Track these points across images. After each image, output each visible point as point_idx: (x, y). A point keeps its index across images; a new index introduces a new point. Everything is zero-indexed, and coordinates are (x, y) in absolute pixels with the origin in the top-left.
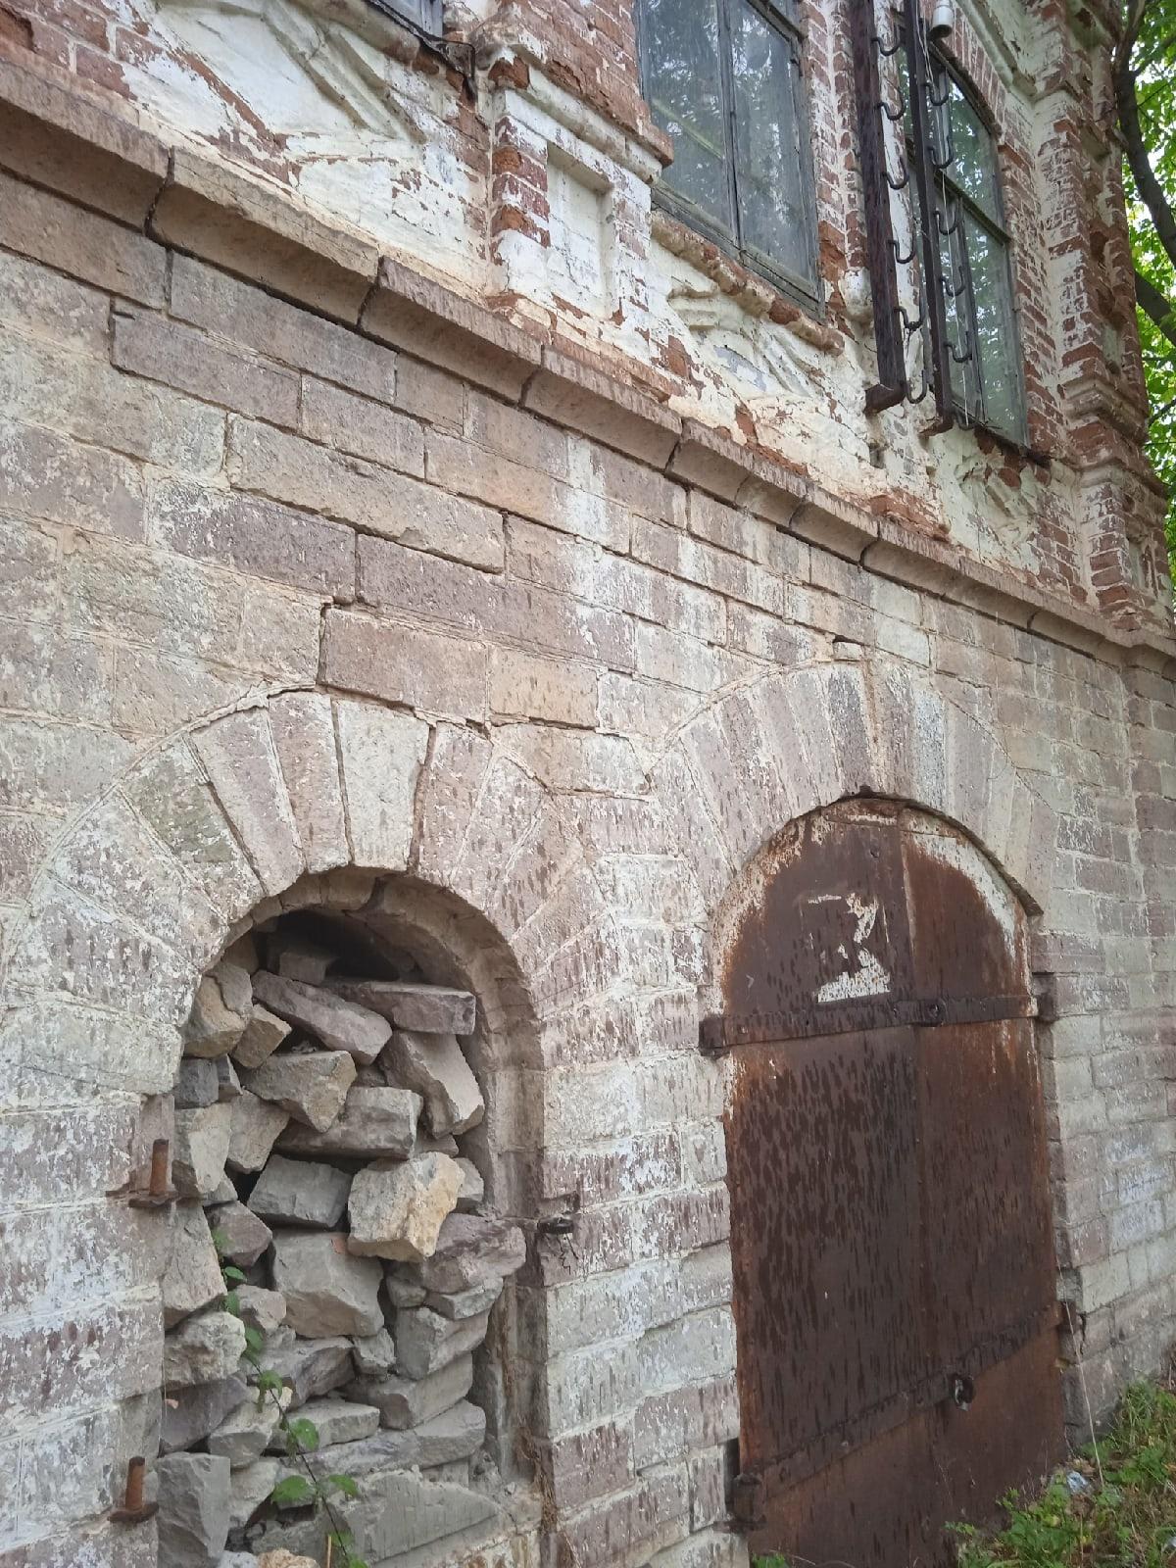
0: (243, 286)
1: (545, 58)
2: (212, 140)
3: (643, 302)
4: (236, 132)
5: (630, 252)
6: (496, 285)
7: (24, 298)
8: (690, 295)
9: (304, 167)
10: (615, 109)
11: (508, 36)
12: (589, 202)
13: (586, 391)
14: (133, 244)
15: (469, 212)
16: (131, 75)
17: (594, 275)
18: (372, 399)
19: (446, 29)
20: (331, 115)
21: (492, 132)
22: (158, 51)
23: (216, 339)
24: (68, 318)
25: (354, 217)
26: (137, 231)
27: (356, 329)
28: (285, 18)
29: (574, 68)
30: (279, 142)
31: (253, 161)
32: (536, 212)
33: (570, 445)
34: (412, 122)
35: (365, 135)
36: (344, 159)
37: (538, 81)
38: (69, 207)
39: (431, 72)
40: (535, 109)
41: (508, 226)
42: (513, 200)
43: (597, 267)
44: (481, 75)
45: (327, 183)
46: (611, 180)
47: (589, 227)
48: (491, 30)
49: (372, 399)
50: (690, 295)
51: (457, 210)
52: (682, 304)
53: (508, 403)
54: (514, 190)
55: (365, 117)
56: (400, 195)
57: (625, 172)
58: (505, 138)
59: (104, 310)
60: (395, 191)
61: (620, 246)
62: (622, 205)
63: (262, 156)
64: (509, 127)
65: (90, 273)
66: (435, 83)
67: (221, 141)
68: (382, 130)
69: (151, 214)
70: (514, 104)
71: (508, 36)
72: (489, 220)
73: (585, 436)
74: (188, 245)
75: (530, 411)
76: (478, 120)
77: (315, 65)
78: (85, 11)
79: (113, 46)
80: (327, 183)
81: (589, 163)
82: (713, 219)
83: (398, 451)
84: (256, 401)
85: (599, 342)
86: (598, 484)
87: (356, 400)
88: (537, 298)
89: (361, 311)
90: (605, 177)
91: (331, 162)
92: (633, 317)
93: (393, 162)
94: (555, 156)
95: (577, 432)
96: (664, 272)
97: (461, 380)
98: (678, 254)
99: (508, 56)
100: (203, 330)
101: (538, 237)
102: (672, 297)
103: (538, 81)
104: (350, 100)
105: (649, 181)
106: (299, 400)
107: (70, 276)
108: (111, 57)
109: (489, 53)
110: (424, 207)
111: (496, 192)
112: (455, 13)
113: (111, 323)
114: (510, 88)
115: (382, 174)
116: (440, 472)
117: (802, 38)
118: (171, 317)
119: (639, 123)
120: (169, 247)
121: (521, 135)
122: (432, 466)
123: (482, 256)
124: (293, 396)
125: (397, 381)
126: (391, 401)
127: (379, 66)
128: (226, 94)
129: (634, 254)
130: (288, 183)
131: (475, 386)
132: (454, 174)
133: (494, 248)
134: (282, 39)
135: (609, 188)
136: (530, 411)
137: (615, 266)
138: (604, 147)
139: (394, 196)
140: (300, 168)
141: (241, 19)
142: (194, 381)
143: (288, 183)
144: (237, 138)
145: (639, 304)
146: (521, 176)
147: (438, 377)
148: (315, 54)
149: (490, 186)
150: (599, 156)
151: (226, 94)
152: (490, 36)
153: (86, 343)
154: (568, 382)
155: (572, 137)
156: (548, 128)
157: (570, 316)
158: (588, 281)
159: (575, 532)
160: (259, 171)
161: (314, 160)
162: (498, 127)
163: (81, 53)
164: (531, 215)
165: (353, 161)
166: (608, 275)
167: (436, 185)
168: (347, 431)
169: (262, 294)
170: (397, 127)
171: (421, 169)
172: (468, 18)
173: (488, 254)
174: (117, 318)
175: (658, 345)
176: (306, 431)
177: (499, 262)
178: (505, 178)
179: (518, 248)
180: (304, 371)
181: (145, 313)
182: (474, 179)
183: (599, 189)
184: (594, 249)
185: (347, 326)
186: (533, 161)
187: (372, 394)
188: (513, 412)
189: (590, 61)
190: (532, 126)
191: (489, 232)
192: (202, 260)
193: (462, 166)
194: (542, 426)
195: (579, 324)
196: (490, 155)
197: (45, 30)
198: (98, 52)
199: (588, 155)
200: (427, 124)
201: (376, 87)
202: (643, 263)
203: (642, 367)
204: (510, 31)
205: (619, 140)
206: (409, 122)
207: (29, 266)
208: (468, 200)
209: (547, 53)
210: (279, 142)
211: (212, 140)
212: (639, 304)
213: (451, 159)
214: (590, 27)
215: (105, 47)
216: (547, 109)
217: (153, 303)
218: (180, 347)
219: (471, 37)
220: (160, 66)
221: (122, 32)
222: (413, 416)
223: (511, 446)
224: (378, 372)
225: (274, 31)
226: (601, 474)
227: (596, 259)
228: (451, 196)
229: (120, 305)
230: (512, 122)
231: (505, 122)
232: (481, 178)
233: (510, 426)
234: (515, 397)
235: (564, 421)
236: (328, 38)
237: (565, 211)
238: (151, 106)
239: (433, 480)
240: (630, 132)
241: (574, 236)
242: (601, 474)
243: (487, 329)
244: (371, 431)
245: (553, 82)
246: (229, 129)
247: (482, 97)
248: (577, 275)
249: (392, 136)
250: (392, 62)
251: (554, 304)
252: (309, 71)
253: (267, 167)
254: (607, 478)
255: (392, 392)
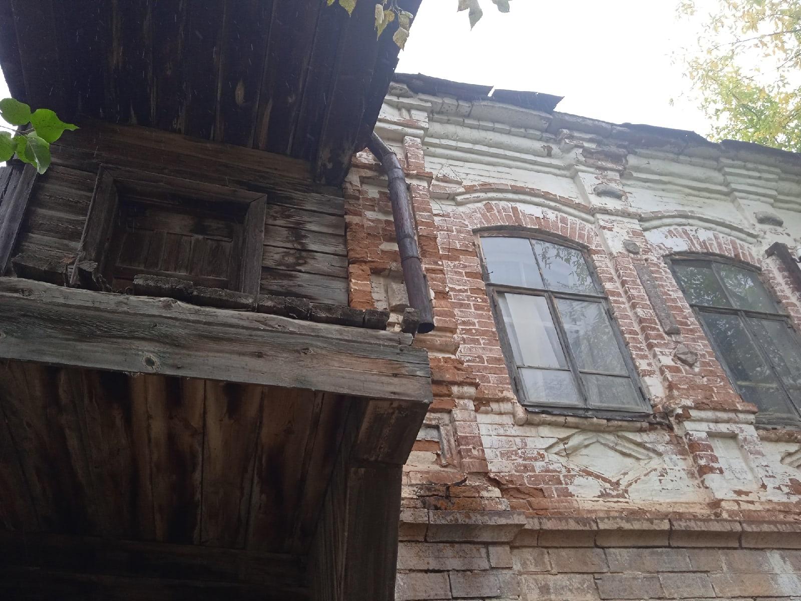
0: (628, 550)
1: (693, 404)
2: (599, 497)
3: (771, 474)
4: (605, 490)
5: (757, 456)
6: (709, 498)
7: (571, 588)
8: (790, 455)
9: (629, 489)
10: (726, 406)
11: (676, 404)
12: (731, 443)
13: (765, 532)
14: (593, 553)
15: (688, 473)
16: (571, 488)
17: (746, 472)
18: (684, 572)
19: (653, 406)
20: (629, 461)
21: (684, 438)
22: (575, 475)
23: (627, 574)
24: (584, 588)
25: (650, 498)
26: (592, 547)
27: (669, 547)
28: (604, 438)
29: (704, 401)
30: (618, 483)
31: (613, 497)
32: (713, 462)
33: (768, 555)
34: (656, 451)
35: (642, 463)
36: (639, 479)
37: (694, 413)
38: (572, 550)
39: (655, 429)
40: (696, 423)
41: (705, 473)
42: (703, 462)
43: (745, 468)
44: (672, 419)
45: (637, 491)
46: (736, 432)
47: (736, 453)
48: (670, 403)
49: (684, 572)
50: (790, 455)
51: (683, 474)
52: (788, 460)
53: (735, 549)
54: (701, 458)
55: (639, 456)
56: (662, 481)
57: (741, 426)
58: (690, 440)
59: (592, 580)
60: (660, 480)
61: (752, 456)
62: (745, 439)
63: (614, 493)
64: (689, 434)
65: (585, 569)
66: (658, 432)
67: (602, 495)
68: (647, 458)
69: (595, 540)
70: (688, 425)
71: (676, 404)
72: (696, 472)
73: (773, 549)
74: (608, 545)
75: (746, 548)
76: (676, 436)
77: (617, 448)
78: (554, 476)
79: (563, 482)
80: (637, 491)
81: (725, 430)
82: (784, 415)
83: (702, 589)
84: (647, 592)
85: (761, 503)
86: (789, 567)
87: (679, 574)
88: (728, 497)
89: (669, 540)
90: (733, 432)
91: (636, 482)
92: (770, 483)
93: (655, 470)
94: (711, 435)
95: (769, 548)
96: (774, 452)
97: (713, 548)
98: (778, 440)
99: (680, 411)
100: (622, 573)
101: (718, 471)
102: (782, 459)
103: (694, 413)
104: (633, 454)
105: (752, 423)
106: (661, 584)
107: (580, 573)
108: (564, 486)
109: (672, 411)
110: (672, 481)
111: (695, 461)
112: (654, 401)
113: (596, 584)
114: (684, 421)
115: (654, 477)
116: (721, 591)
117: (788, 316)
118: (611, 573)
119: (738, 405)
120: (603, 548)
121: (696, 435)
122: (717, 590)
123: (700, 487)
124: (658, 584)
125: (690, 560)
126: (691, 569)
127: (638, 438)
128: (597, 477)
129: (759, 456)
130: (626, 498)
131: (719, 548)
132: (678, 462)
133: (703, 482)
134: (605, 445)
135: (737, 435)
136: (746, 548)
137: (753, 465)
138: (728, 421)
139: (661, 483)
140: (627, 490)
141: (592, 446)
142: (626, 594)
143: (626, 498)
144: (606, 492)
145: (770, 476)
146: (702, 451)
147: (705, 551)
148: (616, 444)
149: (691, 459)
150: (728, 426)
151: (597, 477)
152: (670, 406)
153: (592, 594)
154: (756, 532)
155: (714, 424)
156: (704, 426)
157: (744, 498)
158: (744, 476)
159: (788, 595)
160: (616, 499)
161: (631, 484)
162: (686, 435)
163: (556, 489)
164: (712, 464)
165: (643, 477)
166: (751, 469)
167: (673, 469)
168: (681, 590)
169: (635, 550)
170: (651, 454)
171: (665, 466)
172: (659, 400)
173: (701, 486)
174: (596, 581)
175: (786, 486)
176: (667, 596)
177: (707, 488)
178: (696, 455)
179: (712, 480)
180: (658, 572)
181: (604, 575)
182: (685, 459)
183: (733, 437)
184: (741, 460)
185: (665, 547)
186: (703, 443)
187: (684, 570)
188: (739, 552)
189: (708, 393)
190: (697, 430)
191: (698, 476)
192: (613, 547)
193: (679, 457)
194: (753, 552)
195: (749, 499)
196: (686, 447)
197: (546, 488)
198: (560, 486)
199: (723, 428)
200: (660, 448)
201: (640, 445)
202: (764, 458)
203: (783, 504)
204: (677, 402)
205: (732, 415)
206: (654, 451)
207: (569, 575)
208: (686, 468)
209: (693, 402)
210: (618, 483)
211: (599, 497)
212: (770, 476)
213: (674, 456)
214: (703, 377)
215: (561, 484)
216: (701, 420)
217: (605, 570)
218: (618, 582)
219: (663, 407)
220: (578, 480)
221: (564, 476)
222: (701, 572)
223: (743, 567)
224: (683, 560)
225: (602, 444)
226: (788, 563)
227: (743, 464)
228: (679, 471)
229: (597, 576)
230: (691, 433)
231: (688, 434)
232: (687, 457)
233: (740, 557)
234: (737, 545)
235: (760, 546)
236: (618, 436)
237: (724, 454)
238: (579, 495)
239: (719, 596)
240: (736, 411)
241: (731, 461)
242: (788, 563)
243: (716, 527)
244: (689, 586)
245: (699, 410)
246: (602, 490)
247: (675, 427)
248: (738, 475)
249: (650, 458)
250: (642, 434)
251: (735, 495)
252: (616, 450)
253: (618, 496)
254: (792, 564)
255: (690, 566)
